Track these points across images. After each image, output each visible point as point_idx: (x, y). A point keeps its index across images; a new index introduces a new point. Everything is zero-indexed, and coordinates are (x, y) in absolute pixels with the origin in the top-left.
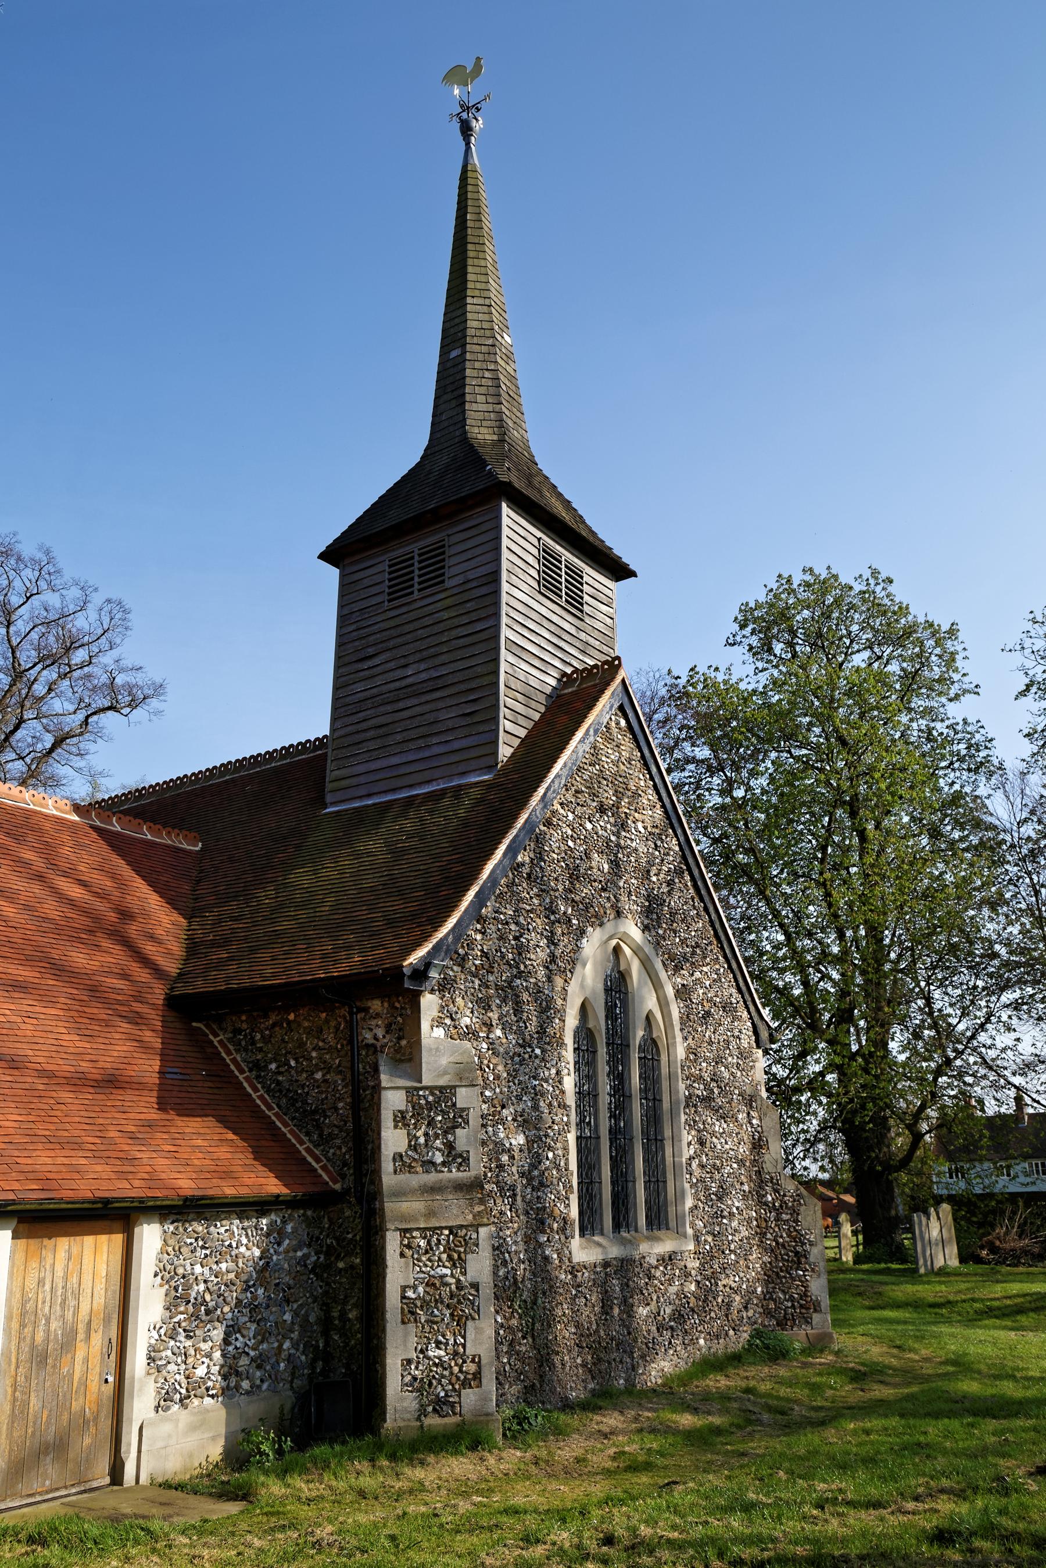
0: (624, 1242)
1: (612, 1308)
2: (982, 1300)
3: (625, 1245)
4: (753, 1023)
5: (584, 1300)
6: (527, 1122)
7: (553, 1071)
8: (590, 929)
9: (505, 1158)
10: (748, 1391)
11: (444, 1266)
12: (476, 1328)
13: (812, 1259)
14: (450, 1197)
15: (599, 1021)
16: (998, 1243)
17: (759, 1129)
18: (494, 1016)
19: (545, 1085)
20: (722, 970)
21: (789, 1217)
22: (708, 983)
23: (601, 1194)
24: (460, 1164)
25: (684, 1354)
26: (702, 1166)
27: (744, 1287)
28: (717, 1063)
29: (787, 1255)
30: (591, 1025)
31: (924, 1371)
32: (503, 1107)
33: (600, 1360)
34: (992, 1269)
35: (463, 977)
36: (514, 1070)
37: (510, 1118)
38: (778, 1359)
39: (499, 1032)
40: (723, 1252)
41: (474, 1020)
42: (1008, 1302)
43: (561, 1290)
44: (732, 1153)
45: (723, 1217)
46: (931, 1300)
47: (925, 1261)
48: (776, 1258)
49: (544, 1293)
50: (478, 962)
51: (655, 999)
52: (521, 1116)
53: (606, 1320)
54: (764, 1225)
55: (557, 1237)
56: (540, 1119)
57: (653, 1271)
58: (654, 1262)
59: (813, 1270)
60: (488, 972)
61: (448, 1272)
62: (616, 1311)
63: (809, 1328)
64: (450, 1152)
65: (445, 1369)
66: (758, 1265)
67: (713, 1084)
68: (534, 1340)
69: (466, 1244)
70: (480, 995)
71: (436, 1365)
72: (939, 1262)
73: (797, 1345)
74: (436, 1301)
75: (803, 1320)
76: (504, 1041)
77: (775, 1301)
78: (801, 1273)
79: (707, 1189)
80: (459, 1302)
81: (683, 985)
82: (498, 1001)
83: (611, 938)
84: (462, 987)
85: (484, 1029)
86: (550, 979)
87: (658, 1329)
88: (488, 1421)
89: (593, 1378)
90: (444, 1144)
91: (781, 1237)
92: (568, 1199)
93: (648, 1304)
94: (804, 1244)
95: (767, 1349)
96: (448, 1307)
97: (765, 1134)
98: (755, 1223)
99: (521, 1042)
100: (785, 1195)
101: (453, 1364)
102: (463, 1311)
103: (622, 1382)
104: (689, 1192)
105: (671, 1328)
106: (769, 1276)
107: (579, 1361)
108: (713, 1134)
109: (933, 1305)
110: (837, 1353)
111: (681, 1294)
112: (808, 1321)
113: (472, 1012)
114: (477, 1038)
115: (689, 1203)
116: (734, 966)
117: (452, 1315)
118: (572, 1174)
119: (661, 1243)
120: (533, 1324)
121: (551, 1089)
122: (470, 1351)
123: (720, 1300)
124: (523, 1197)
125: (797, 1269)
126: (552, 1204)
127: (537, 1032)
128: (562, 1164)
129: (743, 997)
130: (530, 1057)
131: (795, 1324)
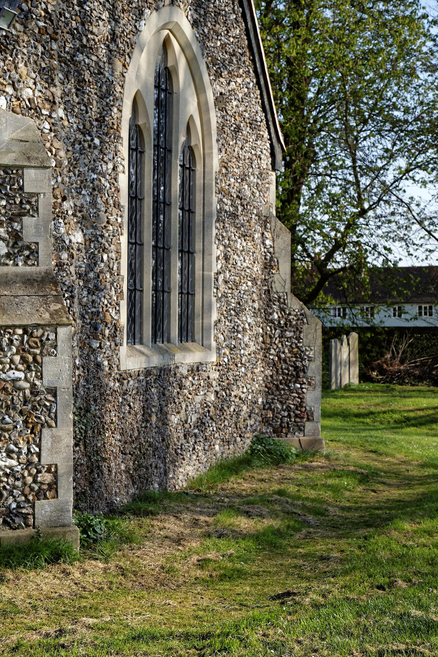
0: (162, 352)
1: (150, 416)
2: (400, 412)
3: (163, 354)
4: (272, 145)
5: (128, 408)
6: (88, 219)
7: (110, 166)
8: (147, 11)
9: (65, 256)
10: (280, 493)
11: (17, 369)
12: (53, 436)
13: (309, 374)
14: (20, 293)
15: (150, 120)
16: (385, 366)
17: (271, 250)
18: (58, 92)
19: (103, 180)
20: (251, 84)
21: (291, 334)
22: (240, 95)
23: (141, 303)
24: (28, 257)
25: (203, 459)
26: (226, 282)
27: (250, 397)
28: (242, 180)
29: (288, 369)
30: (140, 123)
31: (410, 473)
32: (64, 199)
33: (140, 466)
34: (388, 387)
35: (26, 39)
36: (75, 159)
37: (70, 212)
38: (279, 463)
39: (61, 113)
40: (236, 365)
41: (37, 94)
42: (421, 413)
43: (110, 398)
44: (248, 271)
45: (238, 332)
46: (355, 410)
47: (336, 379)
48: (277, 372)
49: (95, 400)
50: (41, 24)
51: (196, 104)
52: (80, 211)
53: (146, 427)
54: (268, 341)
55: (108, 344)
56: (97, 216)
57: (184, 380)
58: (185, 372)
59: (309, 384)
60: (52, 38)
61: (21, 375)
62: (154, 419)
63: (301, 435)
64: (16, 243)
65: (18, 479)
66: (260, 378)
67: (238, 201)
68: (85, 447)
69: (43, 345)
70: (43, 65)
71: (7, 475)
72: (345, 381)
73: (294, 450)
74: (8, 407)
75: (296, 428)
76: (66, 123)
77: (273, 411)
78: (299, 386)
79: (228, 303)
80: (34, 408)
81: (221, 94)
82: (60, 76)
83: (163, 27)
84: (25, 51)
85: (47, 106)
86: (110, 62)
87: (185, 436)
88: (65, 533)
89: (134, 483)
90: (8, 233)
91: (284, 352)
92: (118, 304)
93: (178, 413)
94: (303, 359)
95: (265, 453)
96: (21, 413)
97: (277, 255)
98: (261, 339)
99: (81, 127)
100: (290, 314)
101: (26, 474)
102: (39, 418)
103: (156, 486)
104: (215, 305)
105: (195, 435)
106: (269, 388)
107: (123, 467)
108: (235, 251)
109: (357, 415)
110: (327, 457)
111: (205, 404)
112: (301, 429)
113: (35, 83)
114: (39, 115)
115: (215, 316)
116: (262, 82)
117: (25, 422)
118: (123, 280)
119: (192, 354)
120: (86, 432)
121: (108, 185)
122: (46, 460)
123: (232, 409)
124: (80, 300)
125: (295, 382)
126: (105, 309)
127: (97, 120)
128: (115, 268)
129: (266, 117)
130: (90, 146)
131: (289, 431)
